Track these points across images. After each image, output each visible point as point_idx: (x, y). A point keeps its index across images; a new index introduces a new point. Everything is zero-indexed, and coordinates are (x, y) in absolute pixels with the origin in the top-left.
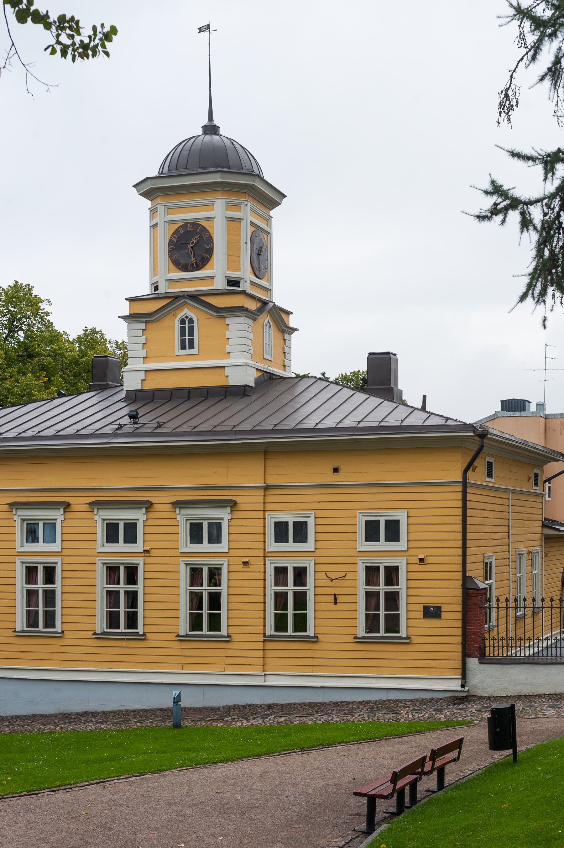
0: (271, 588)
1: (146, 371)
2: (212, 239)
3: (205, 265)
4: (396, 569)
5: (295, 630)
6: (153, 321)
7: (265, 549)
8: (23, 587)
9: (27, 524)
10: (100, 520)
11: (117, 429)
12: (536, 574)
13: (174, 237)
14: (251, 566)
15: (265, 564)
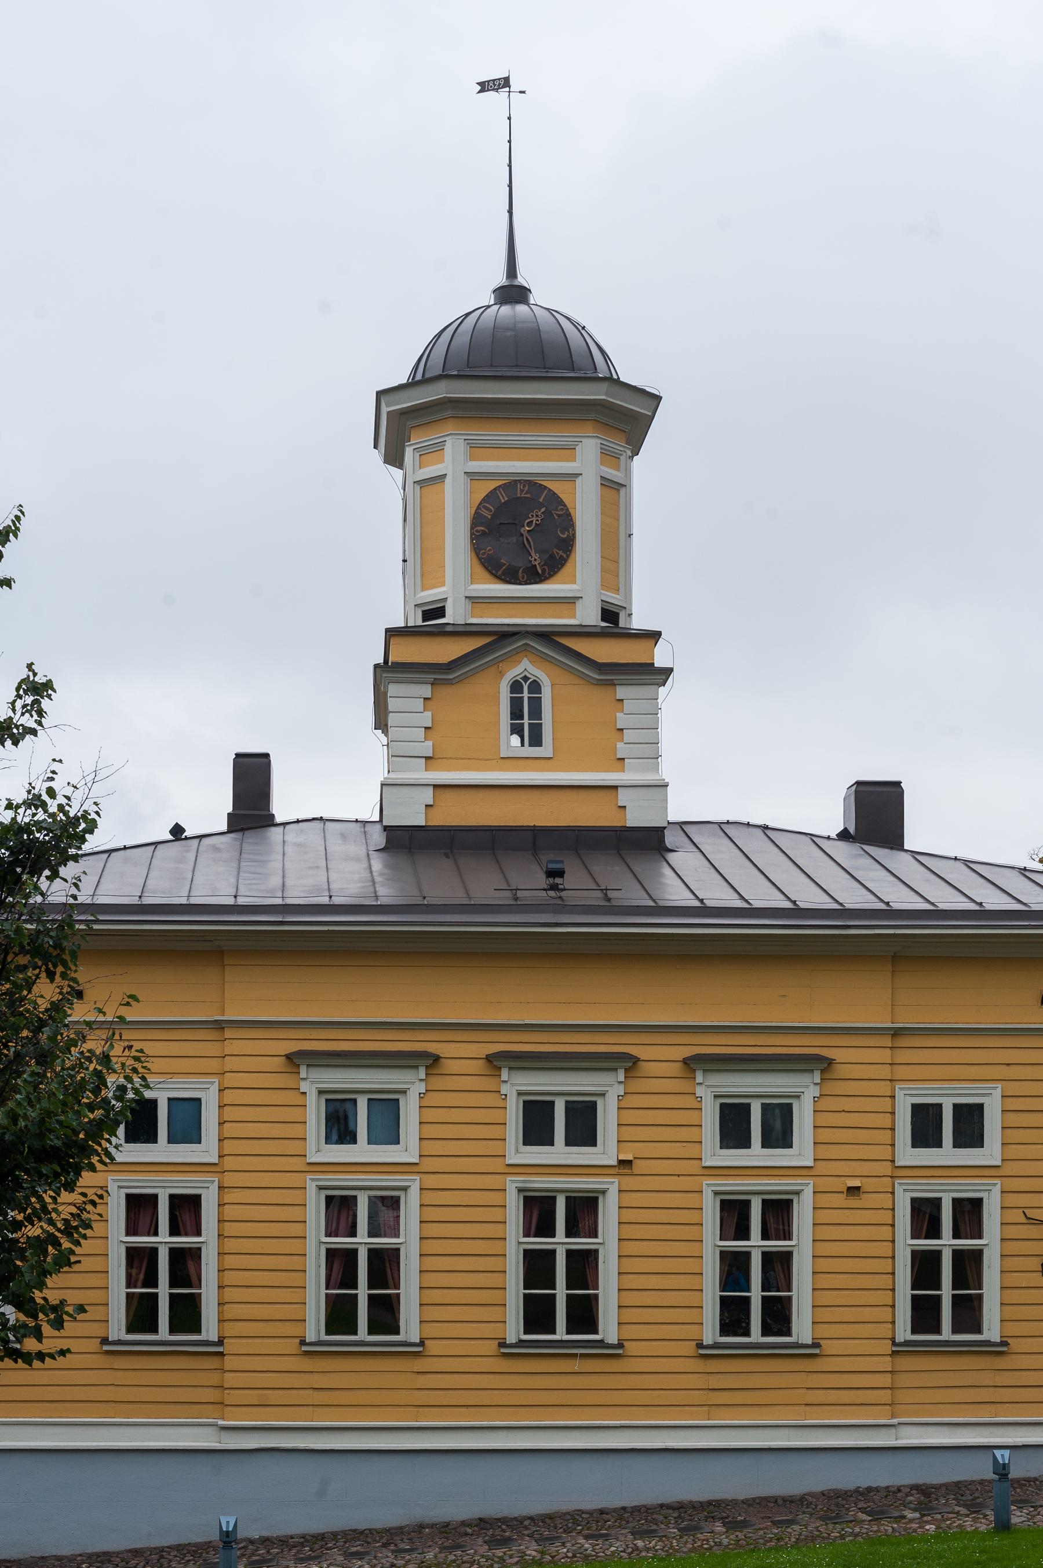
0: (907, 1244)
1: (435, 786)
2: (572, 520)
3: (555, 573)
4: (976, 1204)
6: (449, 682)
7: (893, 1161)
8: (716, 1246)
9: (327, 1100)
10: (515, 1094)
13: (485, 507)
14: (866, 1195)
15: (893, 1193)
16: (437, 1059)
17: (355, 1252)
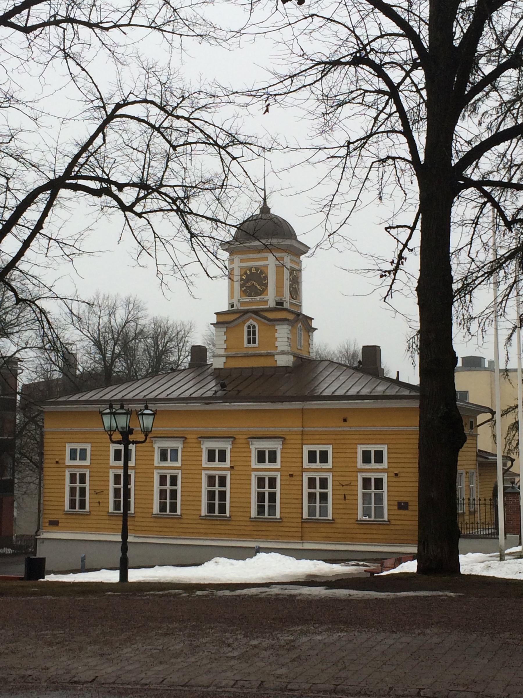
5: (219, 513)
7: (302, 467)
11: (214, 394)
12: (472, 487)
16: (186, 438)
17: (215, 491)
